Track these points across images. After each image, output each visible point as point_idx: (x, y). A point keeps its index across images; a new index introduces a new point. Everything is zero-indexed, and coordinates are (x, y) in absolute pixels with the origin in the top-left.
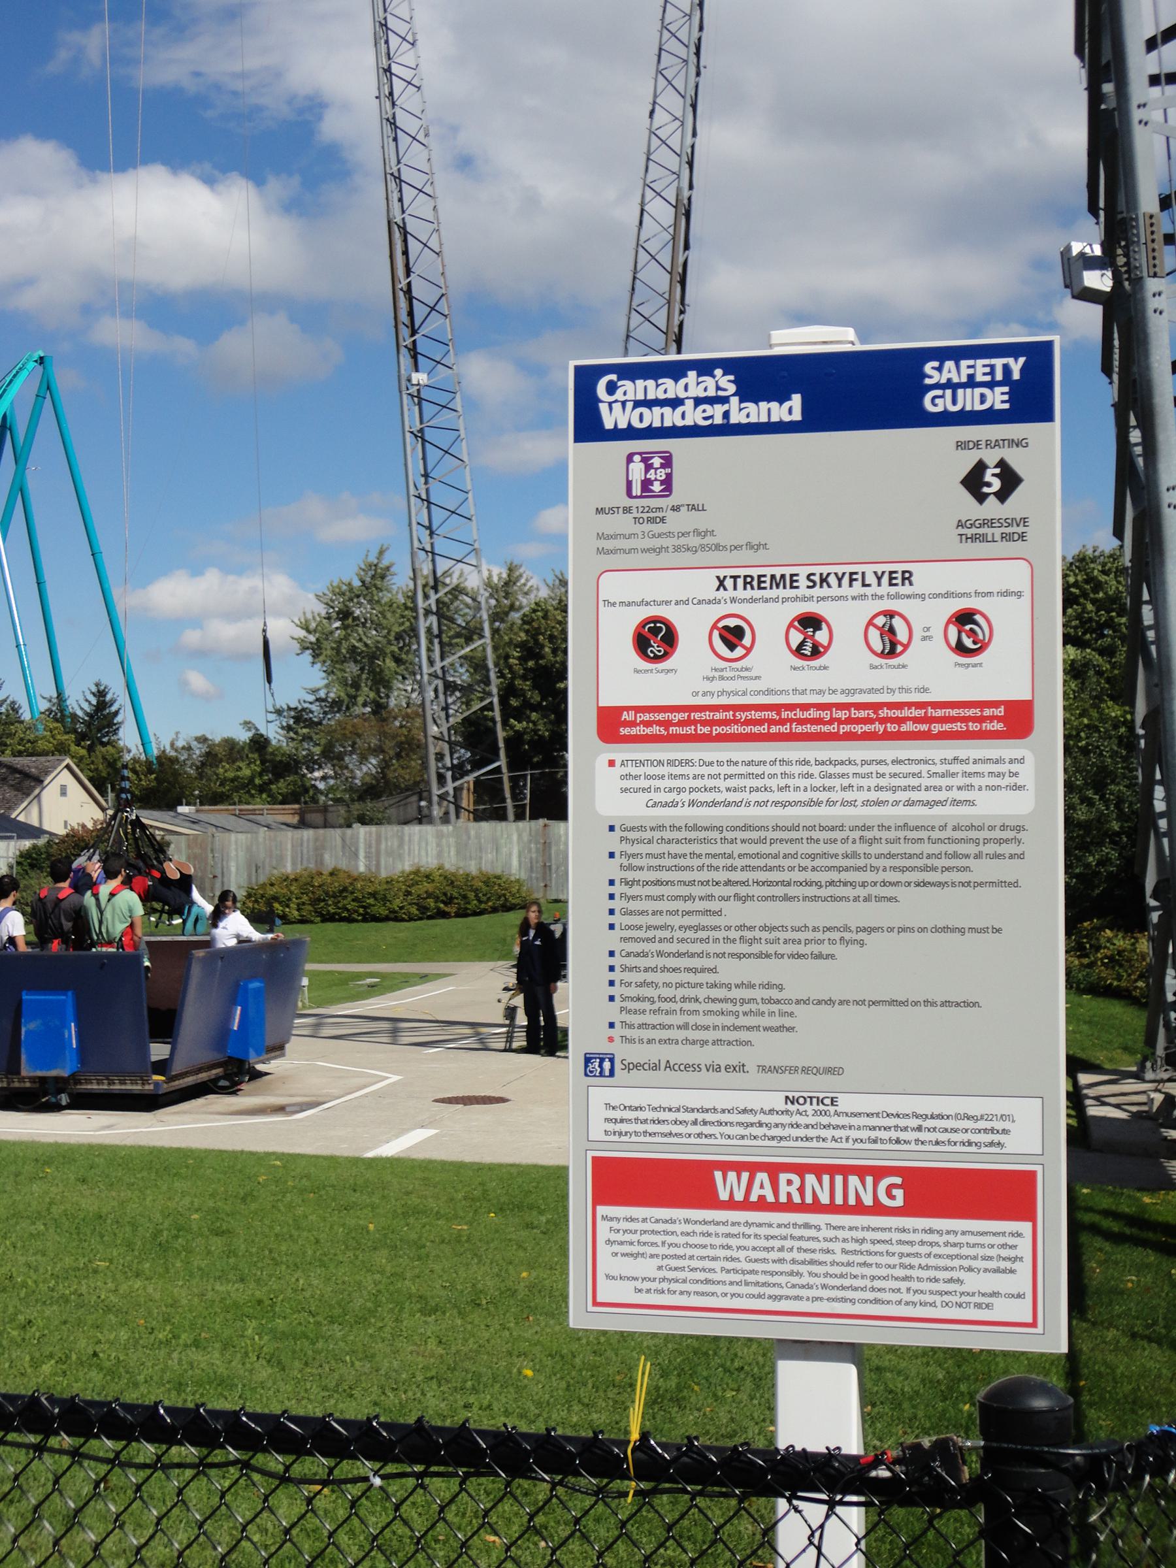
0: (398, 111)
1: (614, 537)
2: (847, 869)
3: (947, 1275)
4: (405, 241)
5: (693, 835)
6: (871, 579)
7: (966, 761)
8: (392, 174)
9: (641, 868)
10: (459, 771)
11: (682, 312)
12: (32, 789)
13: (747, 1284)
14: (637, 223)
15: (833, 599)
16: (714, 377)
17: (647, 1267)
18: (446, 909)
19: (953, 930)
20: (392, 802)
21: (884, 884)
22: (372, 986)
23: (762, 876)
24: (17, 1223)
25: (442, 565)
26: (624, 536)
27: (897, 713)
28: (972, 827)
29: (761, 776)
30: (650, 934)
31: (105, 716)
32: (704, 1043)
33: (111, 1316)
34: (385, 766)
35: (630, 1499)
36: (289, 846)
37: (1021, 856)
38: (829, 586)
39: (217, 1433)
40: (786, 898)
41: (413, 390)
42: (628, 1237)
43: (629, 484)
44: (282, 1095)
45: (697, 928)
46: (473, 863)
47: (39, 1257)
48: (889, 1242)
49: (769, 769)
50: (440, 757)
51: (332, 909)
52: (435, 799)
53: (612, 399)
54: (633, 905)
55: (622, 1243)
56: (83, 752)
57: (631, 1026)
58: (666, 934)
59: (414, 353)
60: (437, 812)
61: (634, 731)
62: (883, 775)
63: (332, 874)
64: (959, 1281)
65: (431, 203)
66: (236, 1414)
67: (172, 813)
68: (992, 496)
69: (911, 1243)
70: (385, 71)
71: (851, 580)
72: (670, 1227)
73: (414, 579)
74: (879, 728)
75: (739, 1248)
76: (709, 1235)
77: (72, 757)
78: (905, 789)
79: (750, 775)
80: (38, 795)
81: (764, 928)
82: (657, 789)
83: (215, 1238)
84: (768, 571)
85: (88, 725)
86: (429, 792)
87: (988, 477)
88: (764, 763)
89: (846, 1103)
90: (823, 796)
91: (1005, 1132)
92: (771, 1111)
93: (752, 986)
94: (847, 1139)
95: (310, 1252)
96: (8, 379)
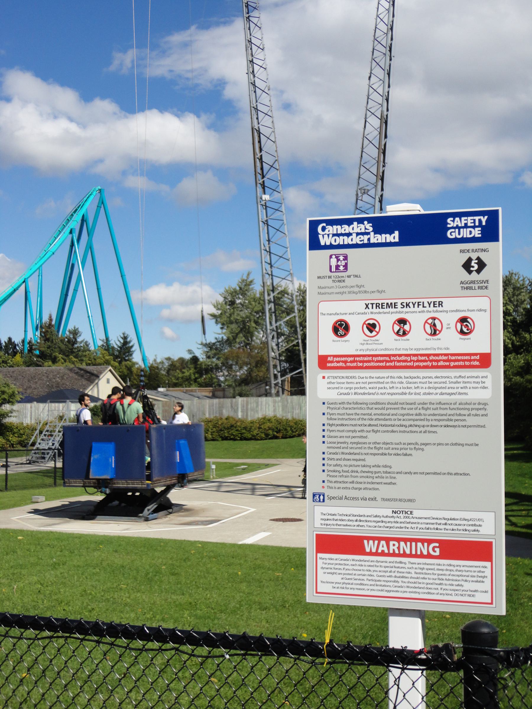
0: (256, 79)
1: (325, 288)
2: (417, 420)
3: (457, 583)
4: (259, 137)
5: (356, 406)
6: (426, 304)
7: (464, 377)
8: (254, 107)
9: (335, 419)
10: (283, 373)
11: (384, 166)
12: (94, 380)
13: (377, 585)
14: (363, 127)
15: (411, 312)
16: (364, 224)
17: (337, 578)
18: (278, 435)
19: (459, 445)
20: (254, 386)
21: (432, 426)
22: (244, 469)
23: (383, 423)
24: (88, 569)
25: (276, 281)
26: (329, 287)
27: (437, 358)
28: (466, 403)
29: (383, 383)
30: (339, 445)
31: (127, 348)
32: (360, 489)
33: (127, 608)
34: (250, 371)
35: (325, 665)
36: (207, 406)
37: (486, 415)
38: (410, 307)
39: (166, 637)
40: (393, 431)
41: (263, 203)
42: (330, 566)
43: (331, 267)
44: (203, 517)
45: (358, 443)
46: (290, 414)
47: (97, 583)
48: (433, 569)
49: (386, 380)
50: (275, 366)
51: (226, 435)
52: (273, 385)
53: (323, 233)
54: (332, 434)
55: (327, 568)
56: (117, 364)
57: (331, 482)
58: (345, 445)
59: (263, 186)
60: (273, 391)
61: (333, 365)
62: (431, 383)
63: (226, 419)
64: (461, 585)
65: (271, 119)
66: (174, 630)
67: (155, 391)
68: (474, 272)
69: (442, 570)
70: (250, 61)
71: (418, 305)
72: (346, 562)
73: (264, 287)
74: (430, 364)
75: (374, 571)
76: (362, 566)
77: (112, 366)
78: (440, 388)
79: (378, 382)
80: (97, 383)
81: (384, 443)
82: (342, 388)
83: (172, 577)
84: (386, 302)
85: (120, 352)
86: (270, 382)
87: (473, 264)
88: (384, 377)
89: (416, 513)
90: (407, 391)
91: (480, 526)
92: (387, 517)
93: (379, 466)
94: (417, 528)
95: (213, 583)
96: (85, 199)
